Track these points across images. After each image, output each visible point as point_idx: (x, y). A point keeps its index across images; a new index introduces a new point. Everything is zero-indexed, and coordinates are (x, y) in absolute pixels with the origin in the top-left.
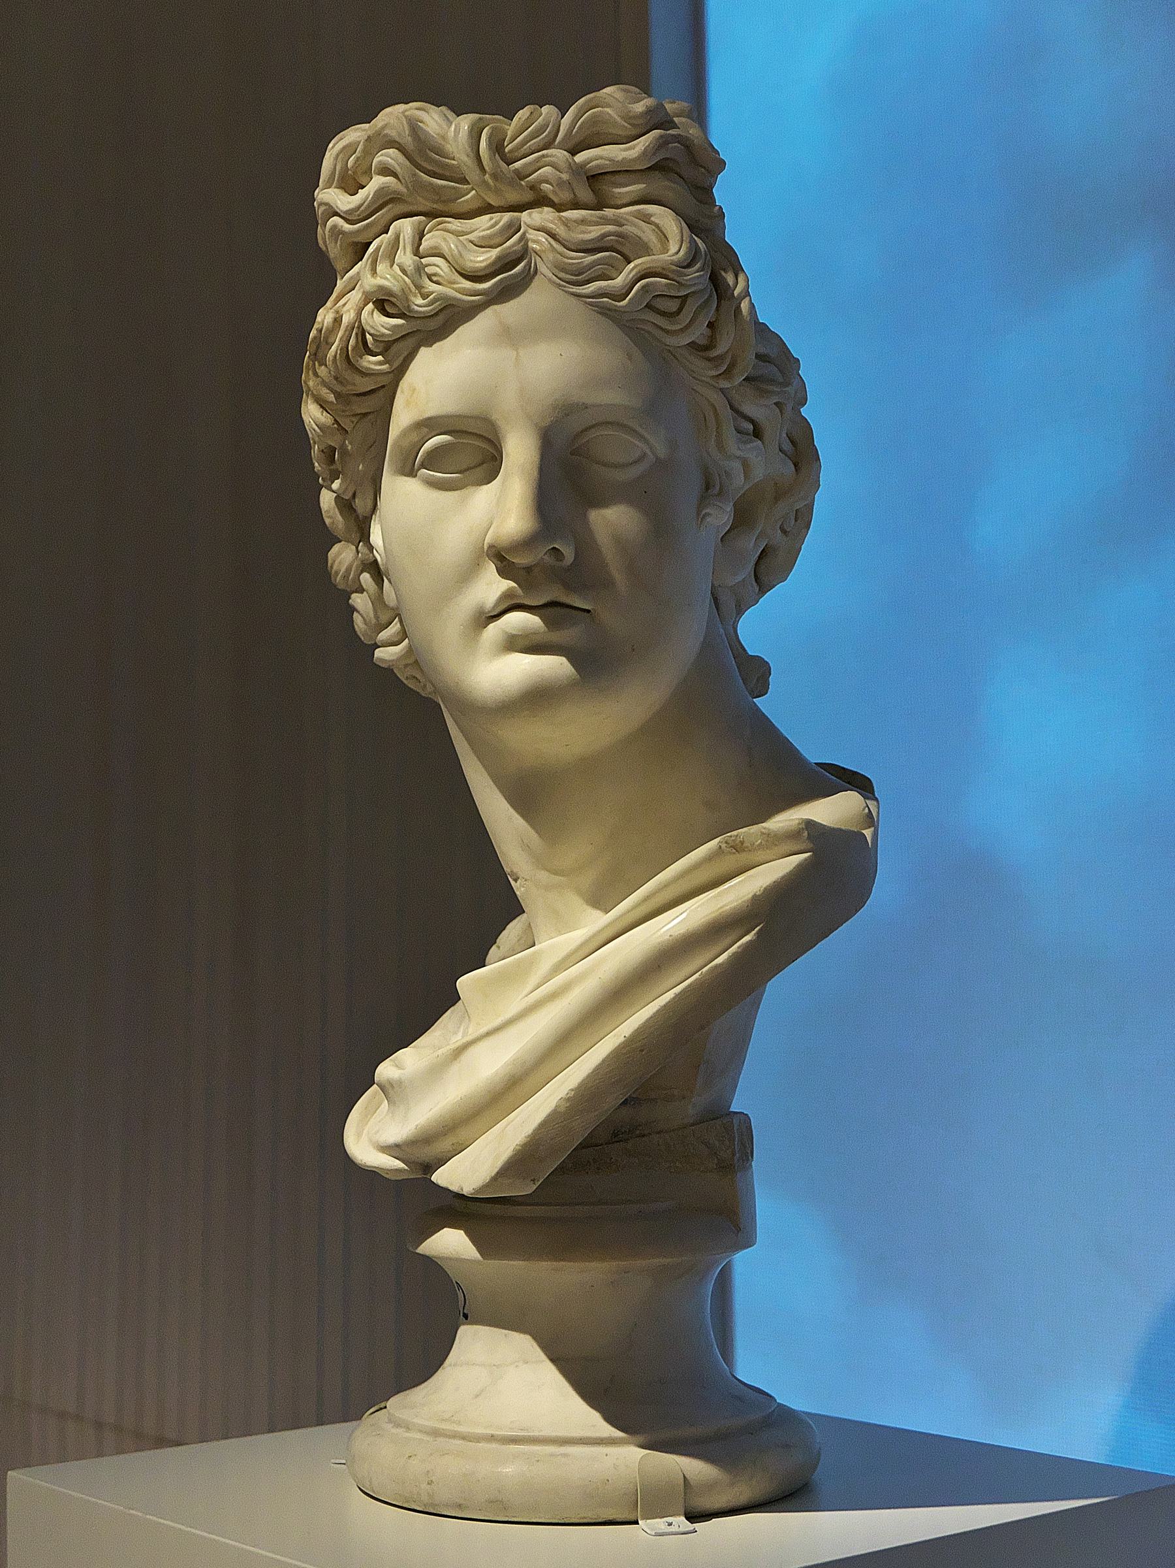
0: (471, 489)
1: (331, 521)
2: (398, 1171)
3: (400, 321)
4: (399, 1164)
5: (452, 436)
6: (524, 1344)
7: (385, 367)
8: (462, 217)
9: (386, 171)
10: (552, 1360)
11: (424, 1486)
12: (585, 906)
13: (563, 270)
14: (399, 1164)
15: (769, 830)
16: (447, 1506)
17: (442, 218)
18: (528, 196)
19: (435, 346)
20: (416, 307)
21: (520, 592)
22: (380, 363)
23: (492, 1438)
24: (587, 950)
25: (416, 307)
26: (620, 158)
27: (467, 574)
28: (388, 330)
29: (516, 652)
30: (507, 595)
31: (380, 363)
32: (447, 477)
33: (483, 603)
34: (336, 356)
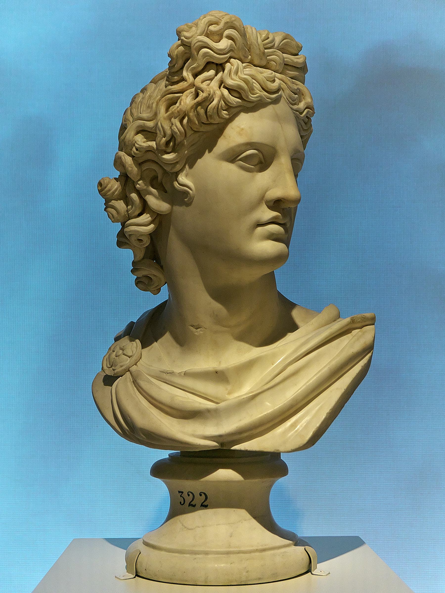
0: (255, 173)
1: (131, 169)
2: (215, 446)
3: (240, 101)
4: (215, 444)
5: (258, 151)
6: (243, 513)
7: (228, 117)
8: (263, 67)
9: (230, 37)
10: (255, 518)
11: (244, 573)
12: (233, 340)
13: (290, 98)
14: (215, 444)
15: (366, 316)
16: (256, 579)
17: (250, 64)
18: (264, 63)
19: (249, 114)
20: (250, 97)
21: (281, 217)
22: (226, 114)
23: (257, 551)
24: (299, 358)
25: (250, 97)
26: (295, 61)
27: (254, 207)
28: (235, 102)
29: (271, 240)
30: (275, 217)
31: (226, 114)
32: (249, 167)
33: (259, 220)
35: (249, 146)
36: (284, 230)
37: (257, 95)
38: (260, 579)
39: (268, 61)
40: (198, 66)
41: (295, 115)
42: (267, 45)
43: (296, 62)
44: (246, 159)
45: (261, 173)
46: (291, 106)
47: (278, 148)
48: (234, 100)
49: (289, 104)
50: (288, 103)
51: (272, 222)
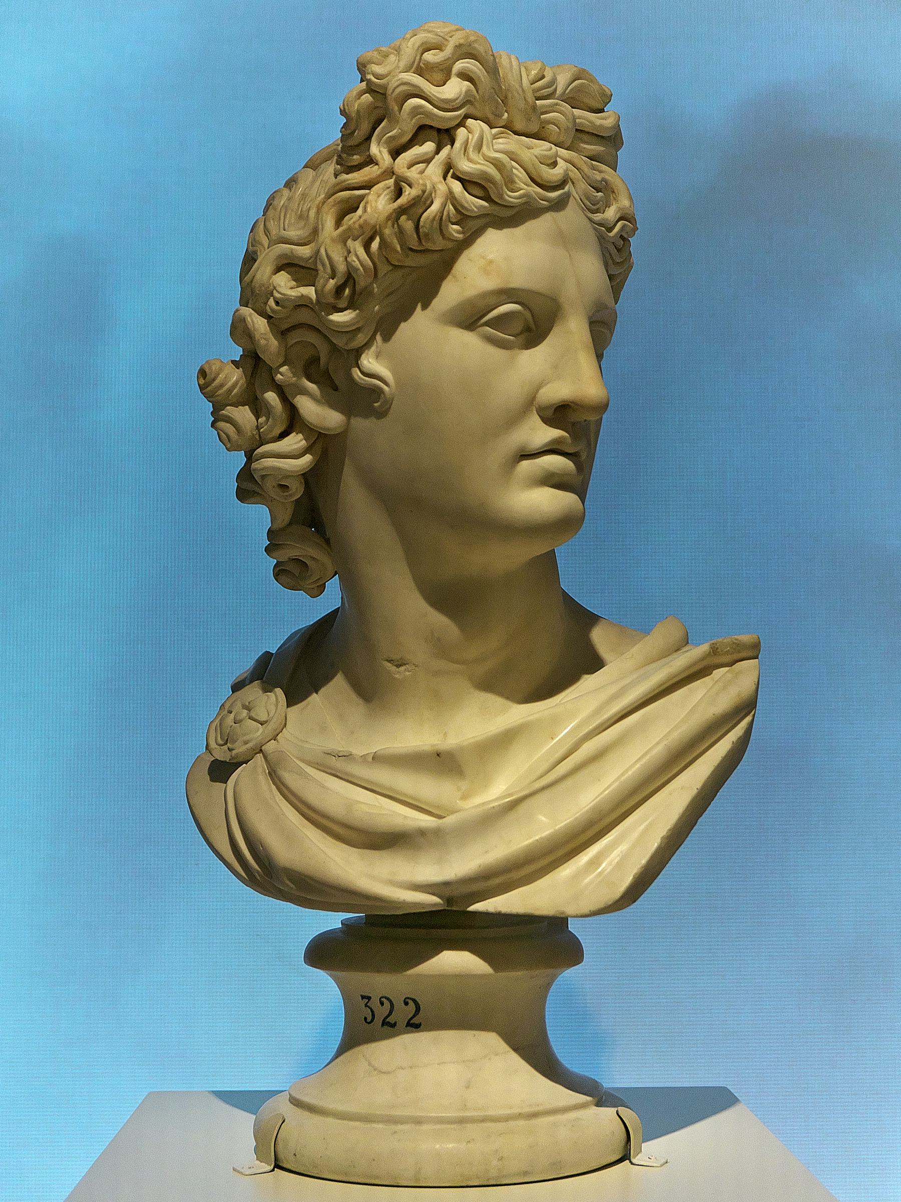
0: (517, 351)
1: (265, 342)
2: (436, 905)
3: (485, 204)
4: (435, 899)
5: (522, 307)
6: (492, 1040)
7: (461, 236)
8: (533, 136)
9: (465, 76)
10: (516, 1049)
11: (495, 1162)
12: (472, 690)
13: (588, 198)
14: (435, 899)
15: (740, 641)
16: (518, 1174)
17: (507, 130)
18: (534, 128)
19: (505, 230)
20: (506, 197)
21: (569, 441)
22: (458, 232)
23: (520, 1116)
24: (606, 725)
25: (506, 197)
26: (598, 124)
27: (514, 419)
28: (476, 207)
29: (548, 486)
30: (558, 441)
31: (458, 232)
32: (504, 338)
33: (524, 447)
34: (435, 216)
35: (505, 297)
36: (574, 467)
37: (521, 192)
38: (526, 1173)
39: (544, 124)
40: (401, 135)
41: (597, 234)
42: (541, 92)
43: (599, 126)
44: (499, 323)
45: (529, 351)
46: (589, 215)
47: (562, 300)
48: (474, 203)
49: (585, 210)
50: (583, 209)
51: (551, 449)
